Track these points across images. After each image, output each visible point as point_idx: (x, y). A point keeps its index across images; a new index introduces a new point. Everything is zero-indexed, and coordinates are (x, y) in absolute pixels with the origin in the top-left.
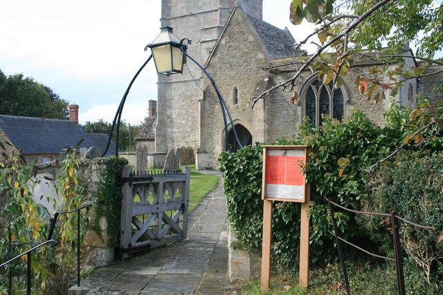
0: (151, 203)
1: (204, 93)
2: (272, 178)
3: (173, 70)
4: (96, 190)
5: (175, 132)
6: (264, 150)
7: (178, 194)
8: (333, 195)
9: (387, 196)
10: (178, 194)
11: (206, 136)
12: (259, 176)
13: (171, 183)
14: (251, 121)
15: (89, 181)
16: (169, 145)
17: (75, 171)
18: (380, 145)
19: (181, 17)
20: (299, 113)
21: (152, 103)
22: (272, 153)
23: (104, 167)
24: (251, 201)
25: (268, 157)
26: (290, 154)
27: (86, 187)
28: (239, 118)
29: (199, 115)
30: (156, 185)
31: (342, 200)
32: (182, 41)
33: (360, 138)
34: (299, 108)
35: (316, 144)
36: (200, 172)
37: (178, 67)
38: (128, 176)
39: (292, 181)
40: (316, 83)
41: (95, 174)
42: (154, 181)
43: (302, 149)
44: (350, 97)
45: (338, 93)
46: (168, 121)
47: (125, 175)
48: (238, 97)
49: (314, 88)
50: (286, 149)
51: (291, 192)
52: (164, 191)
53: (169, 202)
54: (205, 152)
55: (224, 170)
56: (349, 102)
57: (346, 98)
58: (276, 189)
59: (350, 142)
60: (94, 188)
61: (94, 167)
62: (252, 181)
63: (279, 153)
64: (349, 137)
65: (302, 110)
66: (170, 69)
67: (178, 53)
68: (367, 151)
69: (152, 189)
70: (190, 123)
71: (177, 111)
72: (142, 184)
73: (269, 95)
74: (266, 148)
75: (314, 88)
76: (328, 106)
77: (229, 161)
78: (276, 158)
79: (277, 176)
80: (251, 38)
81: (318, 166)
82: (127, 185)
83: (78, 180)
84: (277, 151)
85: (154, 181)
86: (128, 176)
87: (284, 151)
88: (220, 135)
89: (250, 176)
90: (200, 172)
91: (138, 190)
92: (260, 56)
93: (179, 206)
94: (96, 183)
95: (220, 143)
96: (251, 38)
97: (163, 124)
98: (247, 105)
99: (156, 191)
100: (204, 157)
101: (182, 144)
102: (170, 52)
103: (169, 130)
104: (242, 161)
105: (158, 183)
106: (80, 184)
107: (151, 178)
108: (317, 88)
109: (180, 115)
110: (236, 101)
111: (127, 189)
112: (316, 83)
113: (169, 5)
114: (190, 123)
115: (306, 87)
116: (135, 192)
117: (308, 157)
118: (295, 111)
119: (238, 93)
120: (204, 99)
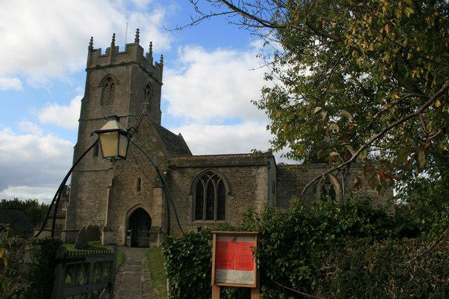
0: (81, 283)
1: (113, 181)
2: (222, 264)
3: (119, 156)
4: (27, 271)
5: (83, 212)
6: (214, 236)
7: (106, 274)
8: (285, 280)
9: (346, 282)
10: (106, 274)
11: (112, 218)
12: (208, 260)
13: (100, 264)
14: (151, 206)
15: (20, 262)
16: (78, 223)
17: (7, 252)
18: (325, 232)
19: (97, 119)
20: (191, 201)
21: (62, 188)
22: (222, 239)
23: (39, 247)
24: (195, 284)
25: (217, 243)
26: (239, 240)
27: (16, 268)
28: (141, 203)
29: (107, 199)
30: (87, 265)
31: (293, 285)
32: (128, 130)
33: (306, 225)
34: (191, 197)
35: (266, 231)
36: (106, 247)
37: (123, 154)
38: (62, 257)
39: (244, 266)
40: (205, 178)
41: (27, 254)
42: (86, 261)
43: (252, 236)
44: (231, 189)
45: (221, 185)
46: (78, 203)
47: (59, 255)
48: (142, 186)
49: (202, 181)
50: (236, 236)
51: (241, 277)
52: (94, 271)
53: (98, 281)
54: (111, 231)
55: (168, 254)
56: (230, 194)
57: (227, 191)
58: (226, 274)
59: (296, 229)
60: (26, 270)
61: (27, 248)
62: (197, 265)
63: (229, 240)
64: (295, 224)
65: (193, 199)
66: (116, 154)
67: (124, 140)
68: (314, 238)
69: (83, 269)
70: (97, 205)
71: (87, 195)
72: (73, 265)
73: (166, 183)
74: (216, 234)
75: (202, 181)
76: (213, 197)
77: (174, 245)
78: (226, 244)
79: (226, 261)
80: (154, 140)
81: (269, 252)
82: (60, 267)
83: (9, 260)
84: (246, 238)
85: (86, 261)
86: (62, 257)
87: (233, 238)
88: (124, 217)
89: (195, 261)
90: (106, 247)
91: (71, 270)
92: (161, 154)
93: (106, 285)
94: (28, 264)
95: (124, 223)
96: (154, 140)
97: (73, 206)
98: (148, 192)
99: (87, 272)
100: (110, 234)
101: (89, 223)
102: (116, 141)
103: (79, 210)
104: (188, 246)
105: (89, 263)
106: (9, 265)
107: (83, 259)
108: (216, 182)
109: (89, 198)
110: (139, 189)
111: (60, 270)
112: (205, 178)
113: (88, 109)
114: (97, 205)
115: (197, 181)
116: (67, 273)
117: (259, 244)
118: (188, 199)
119: (135, 185)
120: (113, 186)
